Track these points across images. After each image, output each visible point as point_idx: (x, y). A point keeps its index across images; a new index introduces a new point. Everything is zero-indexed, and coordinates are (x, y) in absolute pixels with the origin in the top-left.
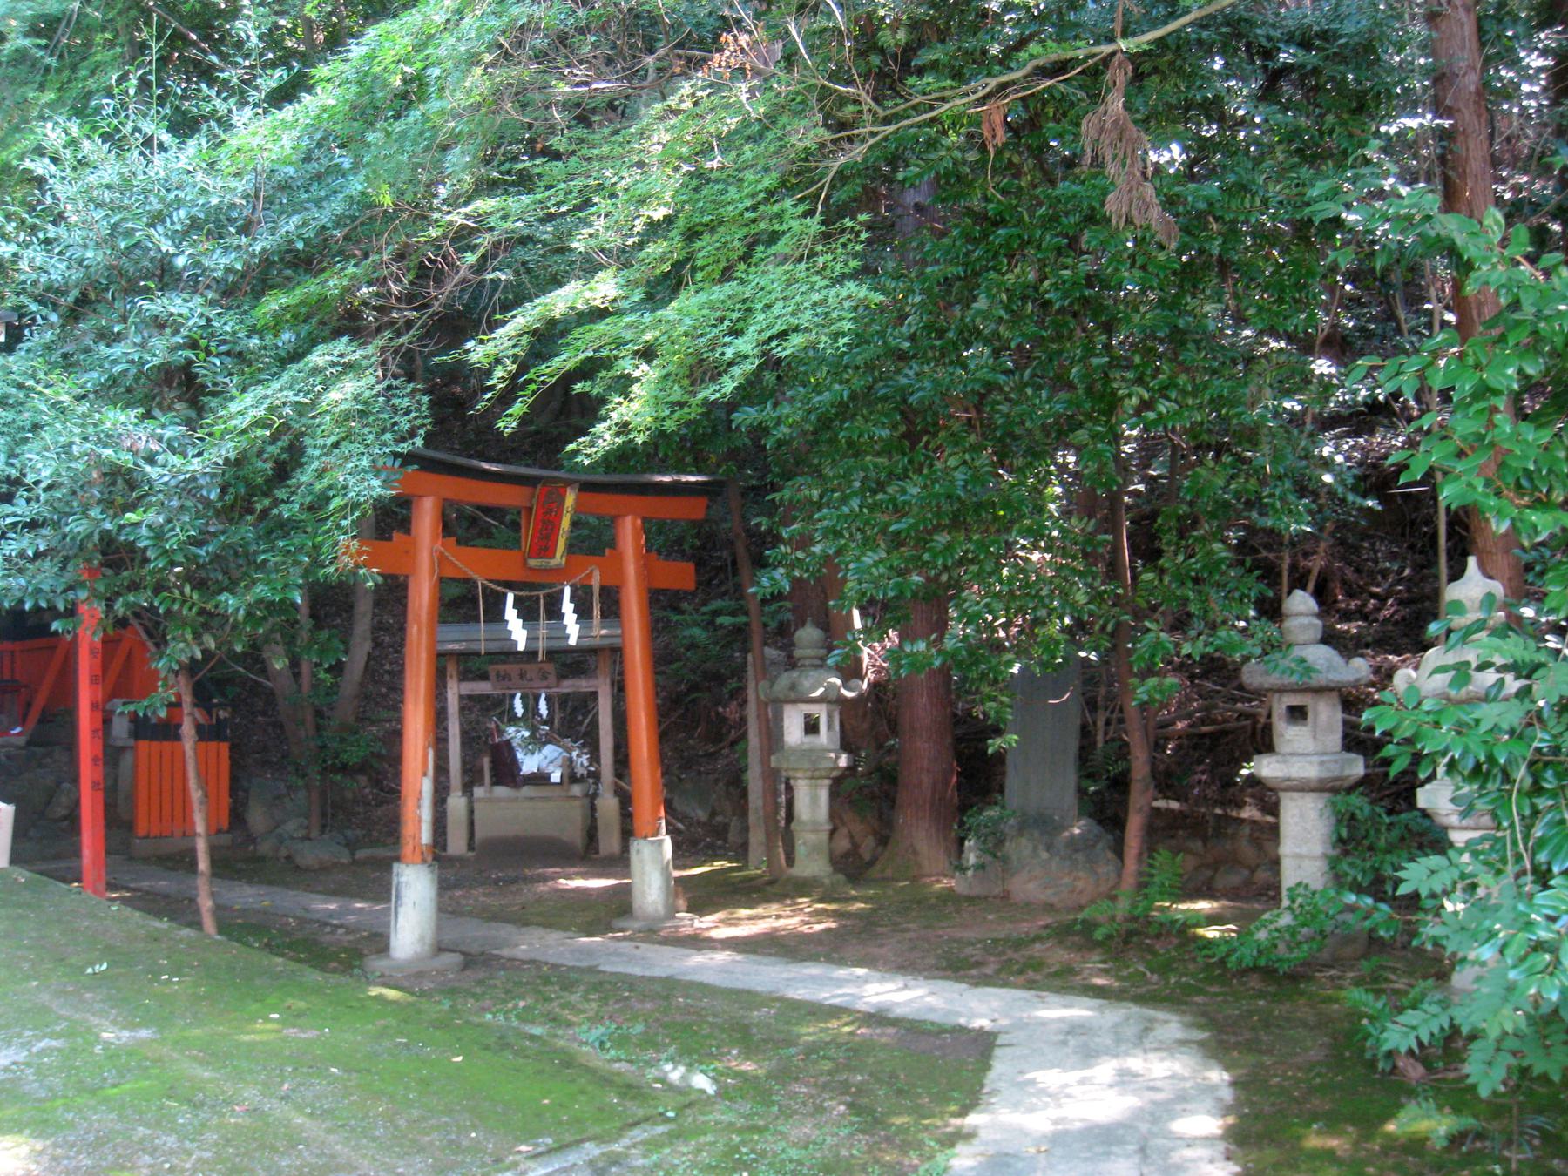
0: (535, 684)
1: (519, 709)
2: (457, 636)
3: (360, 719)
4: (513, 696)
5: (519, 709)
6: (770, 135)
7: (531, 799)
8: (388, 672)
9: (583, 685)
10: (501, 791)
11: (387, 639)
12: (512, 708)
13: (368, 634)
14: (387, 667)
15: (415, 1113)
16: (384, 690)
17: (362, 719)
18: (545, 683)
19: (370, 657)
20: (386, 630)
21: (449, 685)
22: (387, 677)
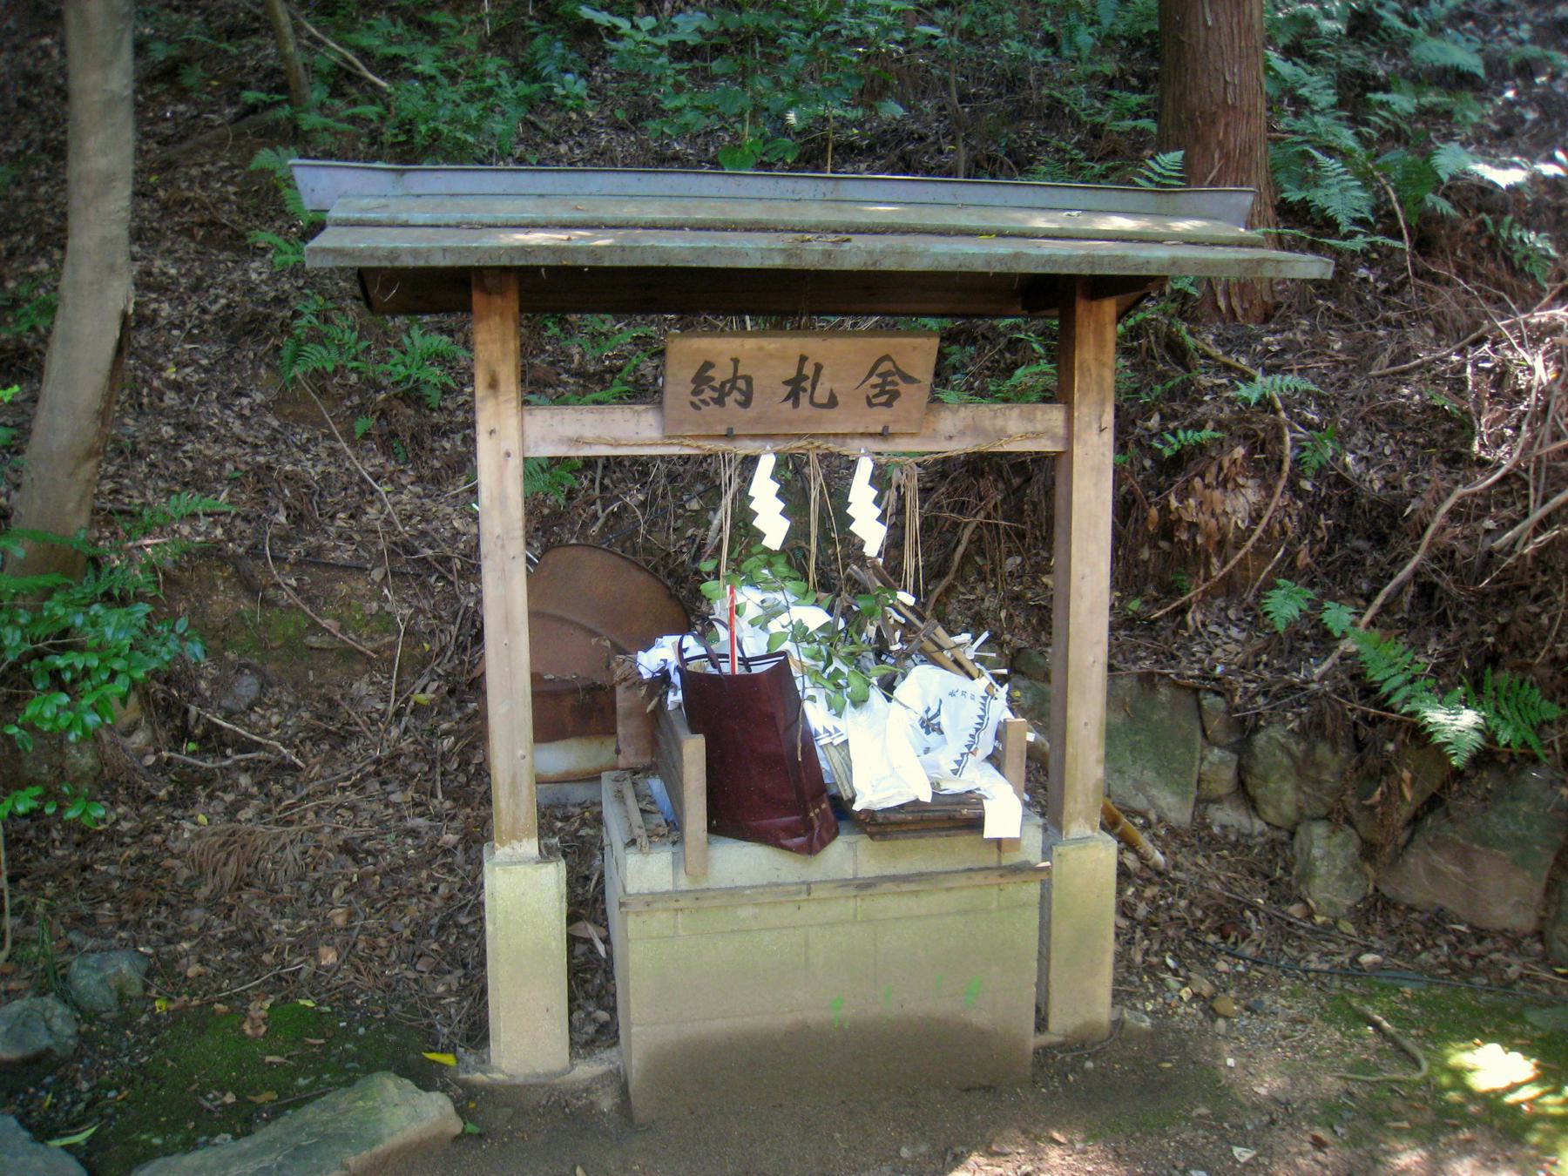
0: (835, 421)
1: (773, 525)
2: (530, 210)
3: (103, 517)
4: (751, 462)
5: (773, 525)
6: (118, 506)
7: (865, 885)
8: (177, 387)
9: (1019, 429)
10: (743, 862)
11: (166, 309)
12: (743, 519)
13: (122, 248)
14: (171, 373)
15: (153, 1085)
16: (167, 431)
17: (113, 515)
18: (877, 419)
19: (131, 324)
20: (162, 289)
21: (485, 418)
22: (171, 399)
